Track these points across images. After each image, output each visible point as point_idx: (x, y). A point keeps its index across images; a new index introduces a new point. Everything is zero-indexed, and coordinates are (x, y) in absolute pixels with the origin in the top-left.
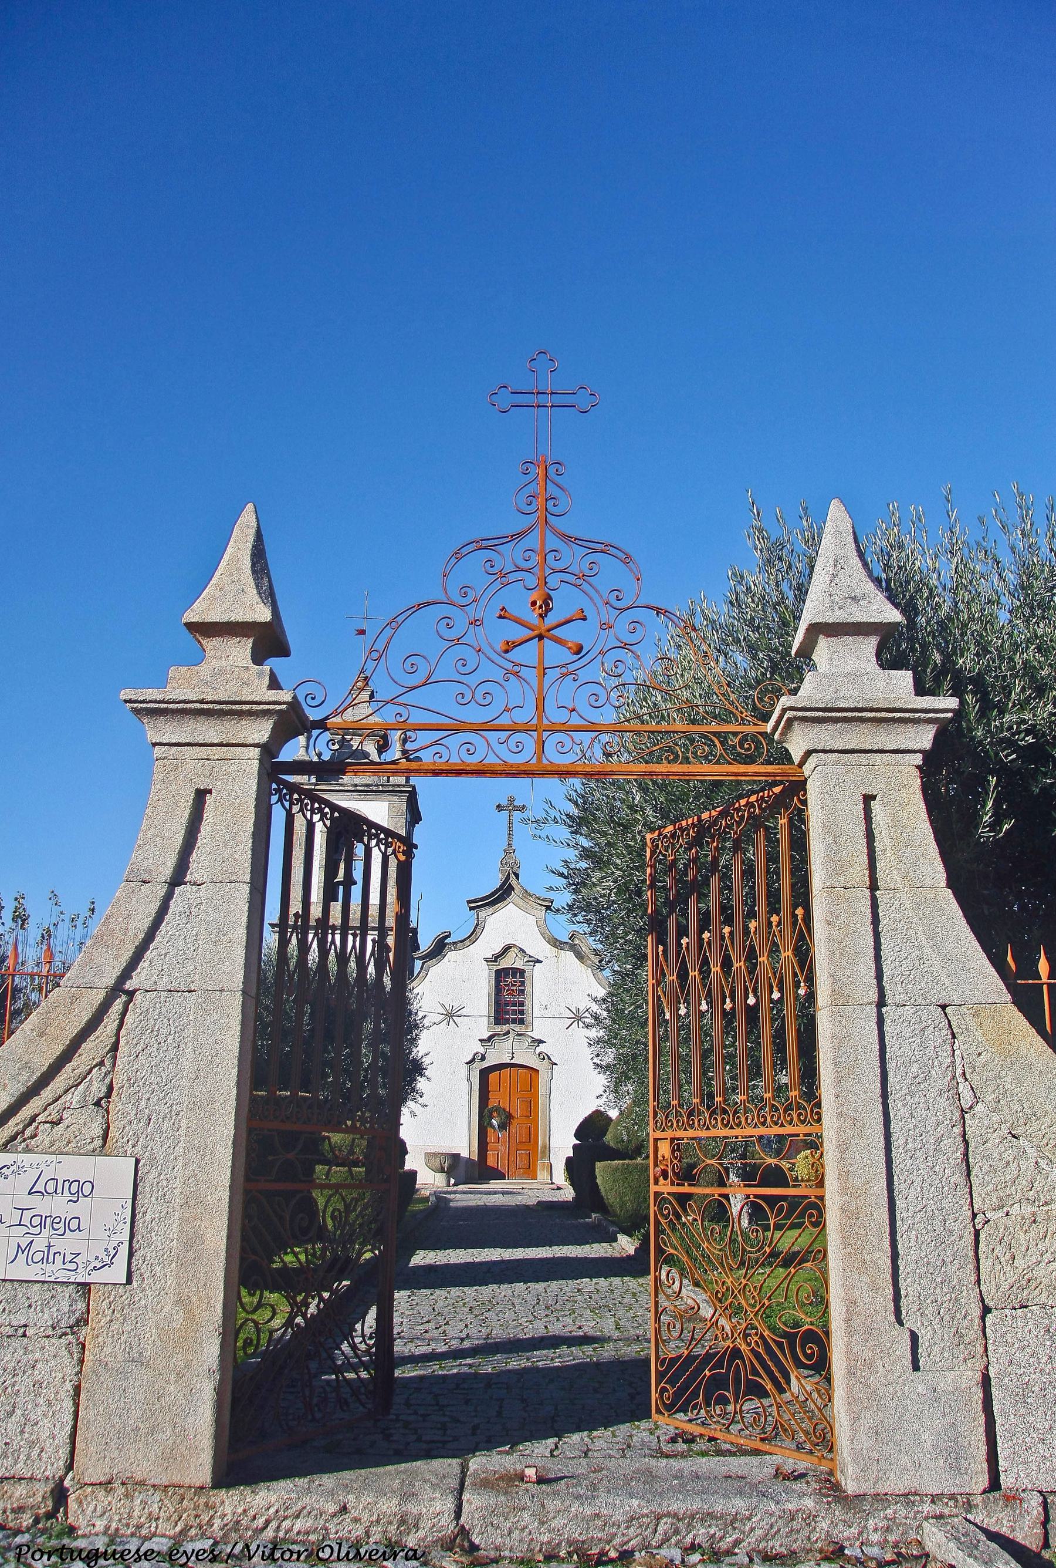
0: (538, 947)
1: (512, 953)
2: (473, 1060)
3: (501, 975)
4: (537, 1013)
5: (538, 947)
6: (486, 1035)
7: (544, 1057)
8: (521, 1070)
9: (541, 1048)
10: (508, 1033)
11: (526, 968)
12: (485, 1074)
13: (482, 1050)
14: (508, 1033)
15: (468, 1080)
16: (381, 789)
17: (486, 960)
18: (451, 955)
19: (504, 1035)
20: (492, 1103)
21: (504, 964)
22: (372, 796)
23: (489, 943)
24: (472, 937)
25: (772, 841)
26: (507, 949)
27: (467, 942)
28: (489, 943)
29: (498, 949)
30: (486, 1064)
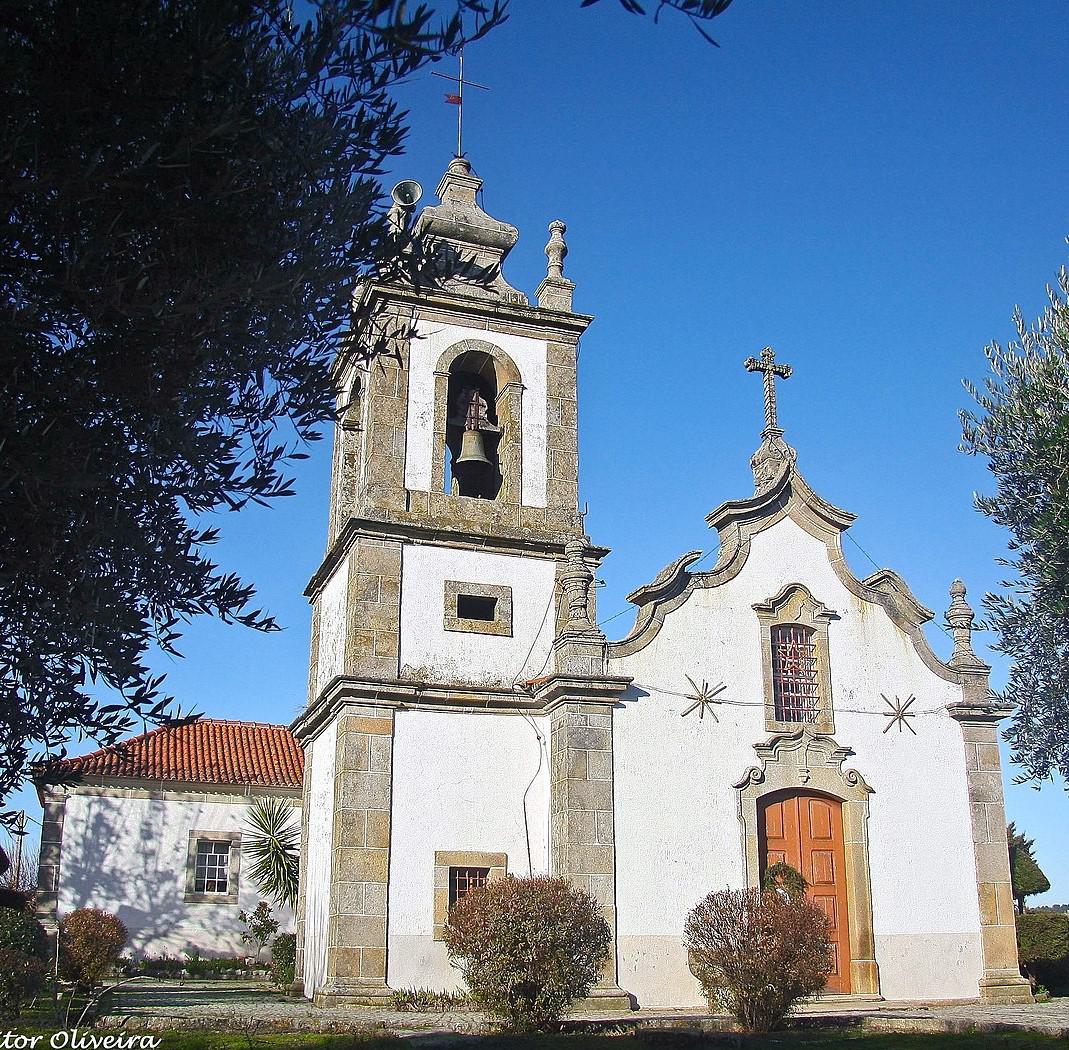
0: (831, 591)
1: (798, 599)
2: (746, 783)
3: (780, 634)
4: (838, 702)
5: (831, 591)
6: (765, 738)
7: (854, 778)
8: (816, 803)
9: (849, 764)
10: (800, 735)
11: (818, 626)
12: (763, 803)
13: (758, 763)
14: (800, 735)
15: (740, 817)
16: (538, 316)
17: (758, 608)
18: (698, 595)
19: (796, 737)
20: (771, 863)
21: (784, 616)
22: (516, 326)
23: (759, 579)
24: (732, 567)
25: (406, 288)
26: (792, 589)
27: (724, 575)
28: (759, 579)
29: (774, 592)
30: (766, 789)
